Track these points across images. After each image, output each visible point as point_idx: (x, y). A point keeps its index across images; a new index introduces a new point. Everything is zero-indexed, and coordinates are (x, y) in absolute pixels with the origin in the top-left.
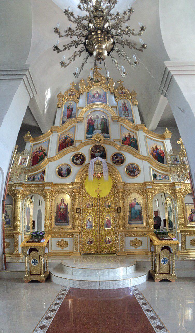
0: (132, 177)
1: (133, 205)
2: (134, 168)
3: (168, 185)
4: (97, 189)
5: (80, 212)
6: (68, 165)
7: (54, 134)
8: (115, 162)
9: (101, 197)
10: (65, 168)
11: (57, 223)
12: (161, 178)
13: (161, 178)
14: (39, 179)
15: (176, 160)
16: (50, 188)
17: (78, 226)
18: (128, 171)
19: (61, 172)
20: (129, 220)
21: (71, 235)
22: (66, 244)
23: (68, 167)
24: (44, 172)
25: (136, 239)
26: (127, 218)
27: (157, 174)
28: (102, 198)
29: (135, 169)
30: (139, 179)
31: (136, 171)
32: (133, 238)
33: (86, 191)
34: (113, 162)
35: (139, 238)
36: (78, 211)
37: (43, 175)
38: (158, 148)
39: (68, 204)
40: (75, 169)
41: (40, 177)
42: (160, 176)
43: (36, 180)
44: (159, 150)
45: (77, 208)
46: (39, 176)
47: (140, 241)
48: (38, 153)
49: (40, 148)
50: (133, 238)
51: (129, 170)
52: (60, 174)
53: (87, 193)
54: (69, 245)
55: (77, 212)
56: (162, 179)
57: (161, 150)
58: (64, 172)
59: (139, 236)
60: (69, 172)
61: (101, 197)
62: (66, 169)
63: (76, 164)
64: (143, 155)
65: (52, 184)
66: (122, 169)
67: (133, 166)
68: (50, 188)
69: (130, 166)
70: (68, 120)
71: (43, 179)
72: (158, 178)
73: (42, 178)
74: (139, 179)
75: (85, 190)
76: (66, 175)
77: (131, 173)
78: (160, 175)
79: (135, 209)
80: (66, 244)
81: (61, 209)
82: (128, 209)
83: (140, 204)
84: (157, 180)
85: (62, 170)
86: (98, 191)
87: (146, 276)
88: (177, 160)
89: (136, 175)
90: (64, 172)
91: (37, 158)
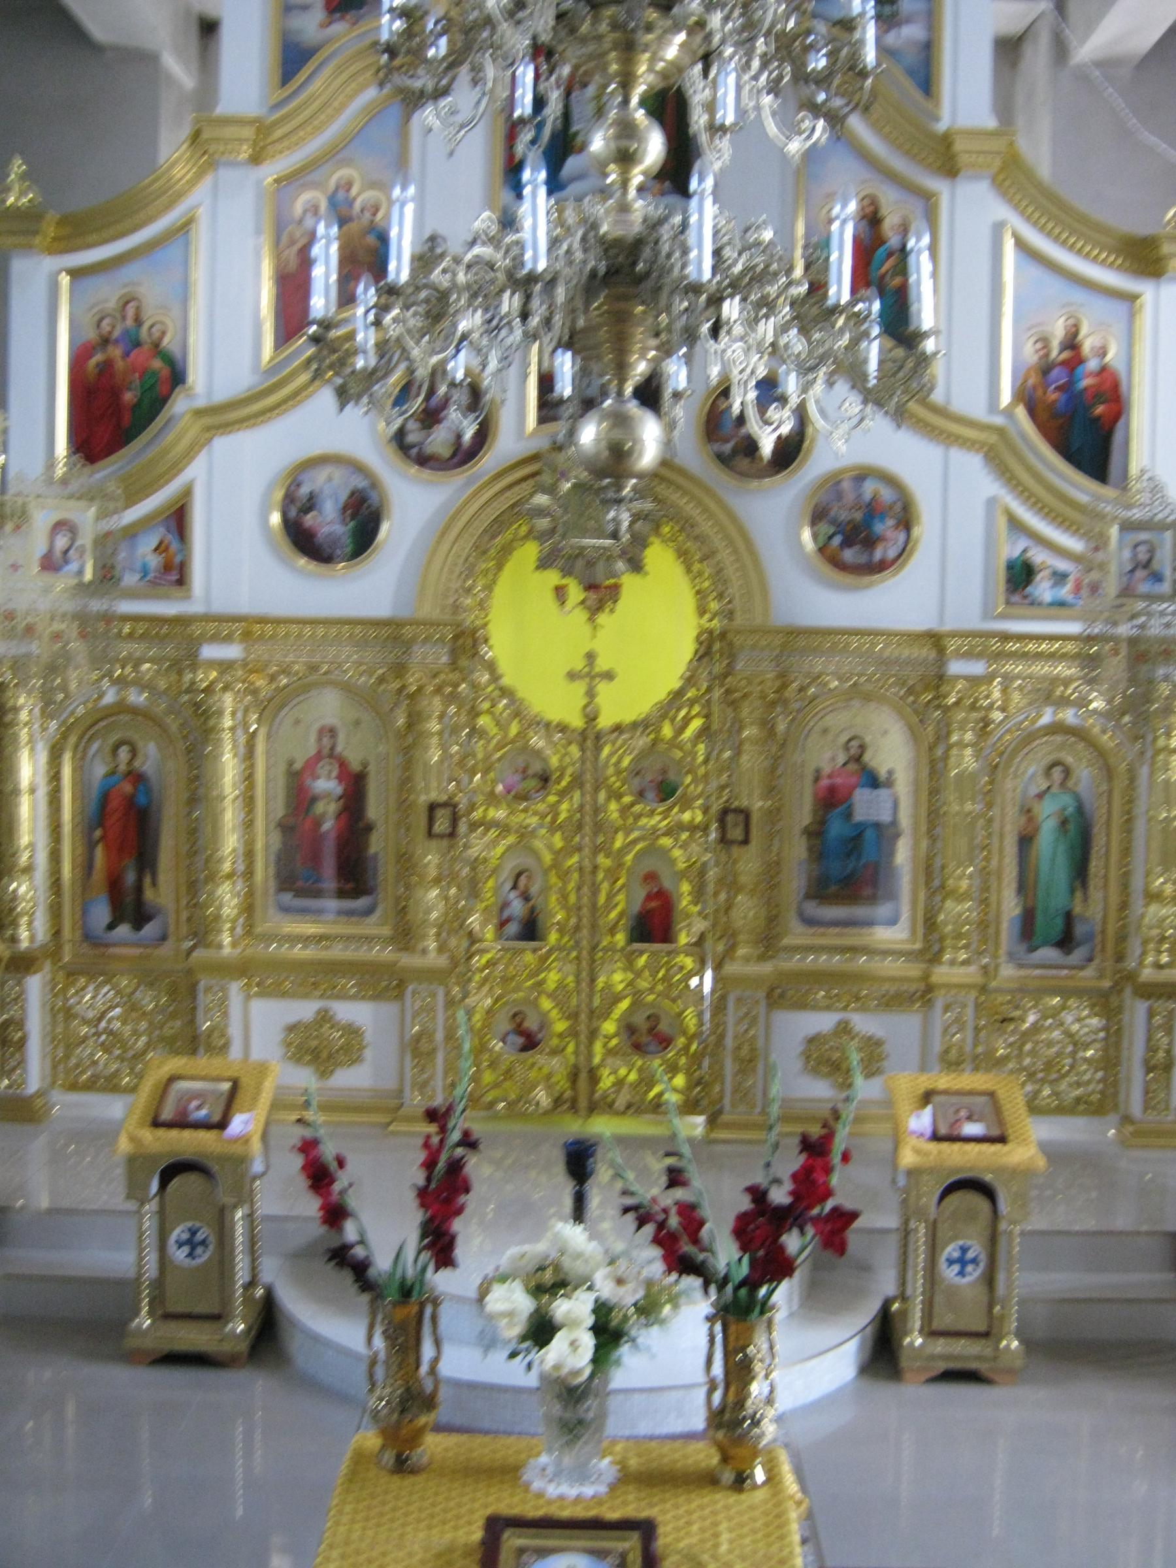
0: (849, 579)
1: (673, 199)
2: (873, 510)
3: (799, 1261)
4: (602, 687)
5: (452, 835)
6: (358, 467)
7: (226, 175)
8: (728, 448)
9: (605, 721)
10: (334, 491)
11: (287, 898)
12: (1065, 592)
13: (1065, 592)
14: (145, 572)
15: (1147, 565)
16: (232, 651)
17: (440, 927)
18: (825, 528)
19: (309, 520)
20: (808, 896)
21: (384, 983)
22: (350, 1048)
23: (360, 483)
24: (178, 518)
25: (844, 1029)
26: (795, 881)
27: (1039, 556)
28: (618, 729)
29: (883, 516)
30: (899, 604)
31: (889, 534)
32: (822, 1022)
33: (495, 678)
34: (716, 447)
35: (865, 1024)
36: (441, 825)
37: (175, 546)
38: (1088, 345)
39: (365, 765)
40: (414, 505)
41: (154, 561)
42: (1060, 578)
43: (130, 579)
44: (1092, 365)
45: (432, 808)
46: (146, 549)
47: (352, 1031)
48: (116, 352)
49: (130, 311)
50: (822, 1022)
51: (833, 522)
52: (303, 540)
53: (505, 692)
54: (368, 1053)
55: (430, 834)
56: (1070, 598)
57: (1104, 369)
58: (328, 521)
59: (863, 1009)
60: (365, 520)
61: (605, 721)
62: (344, 496)
63: (424, 460)
64: (958, 405)
65: (248, 627)
66: (776, 518)
67: (870, 488)
68: (232, 651)
69: (846, 485)
70: (338, 27)
71: (175, 573)
72: (1043, 590)
73: (167, 567)
74: (899, 604)
75: (491, 666)
76: (349, 550)
77: (847, 543)
78: (1062, 565)
79: (848, 815)
80: (350, 1048)
81: (314, 799)
82: (803, 813)
83: (889, 783)
84: (1032, 604)
85: (311, 504)
86: (590, 674)
87: (852, 1347)
88: (1155, 565)
89: (881, 567)
90: (328, 521)
91: (115, 393)
